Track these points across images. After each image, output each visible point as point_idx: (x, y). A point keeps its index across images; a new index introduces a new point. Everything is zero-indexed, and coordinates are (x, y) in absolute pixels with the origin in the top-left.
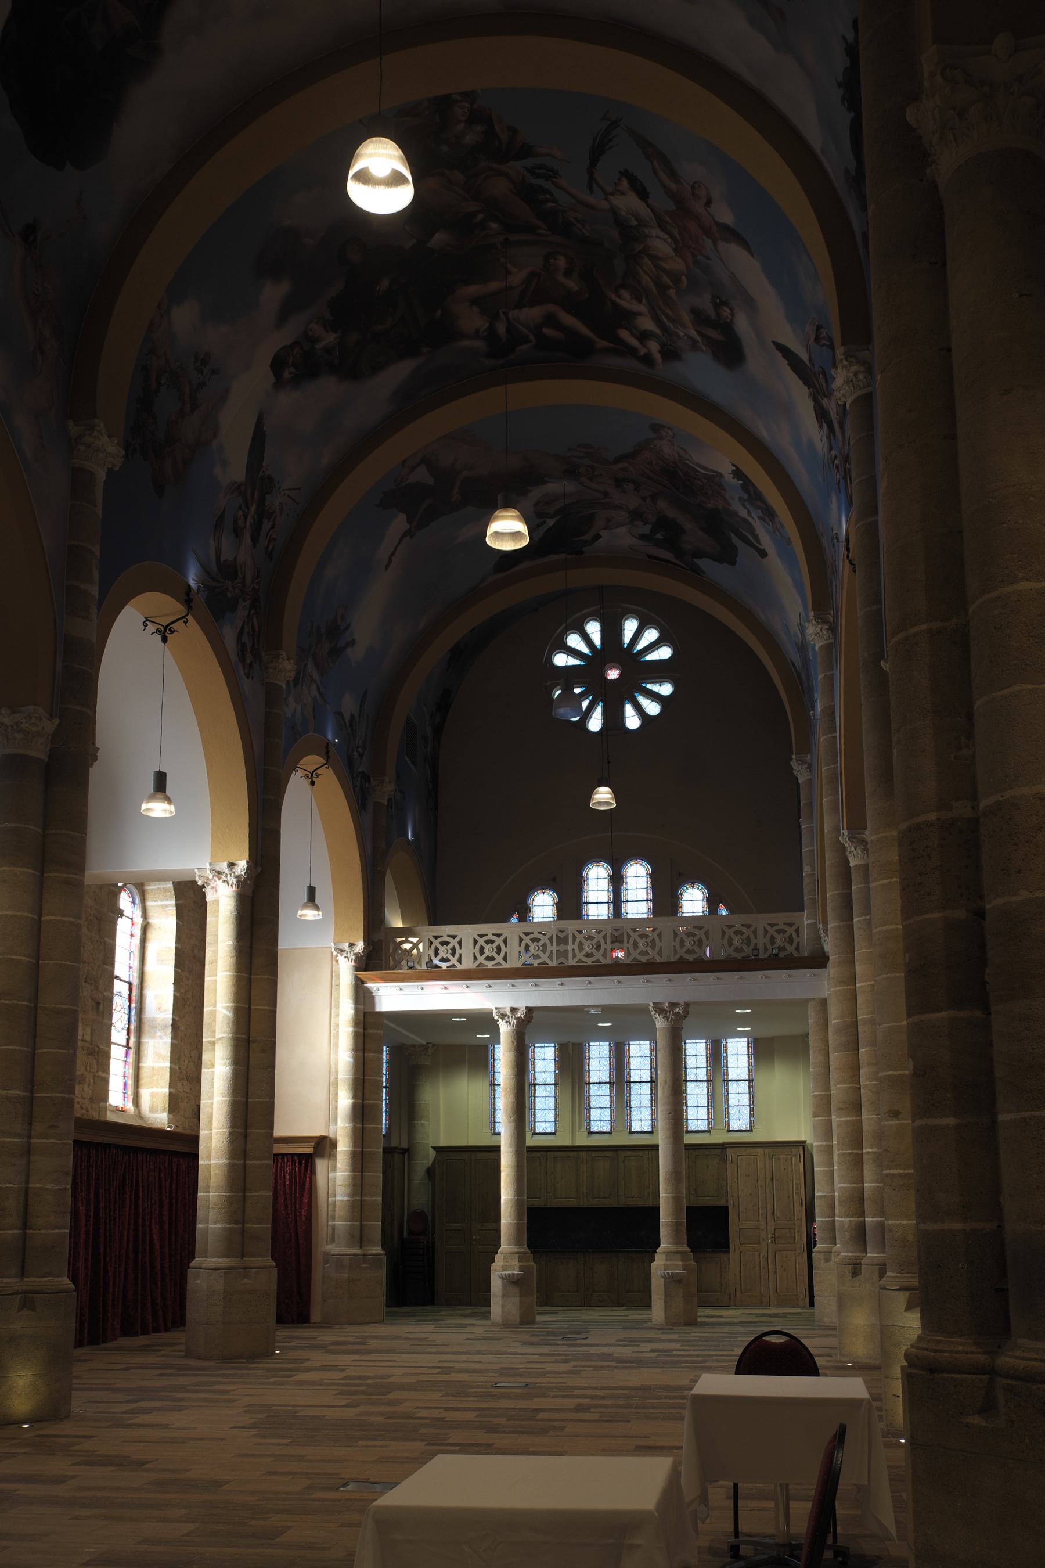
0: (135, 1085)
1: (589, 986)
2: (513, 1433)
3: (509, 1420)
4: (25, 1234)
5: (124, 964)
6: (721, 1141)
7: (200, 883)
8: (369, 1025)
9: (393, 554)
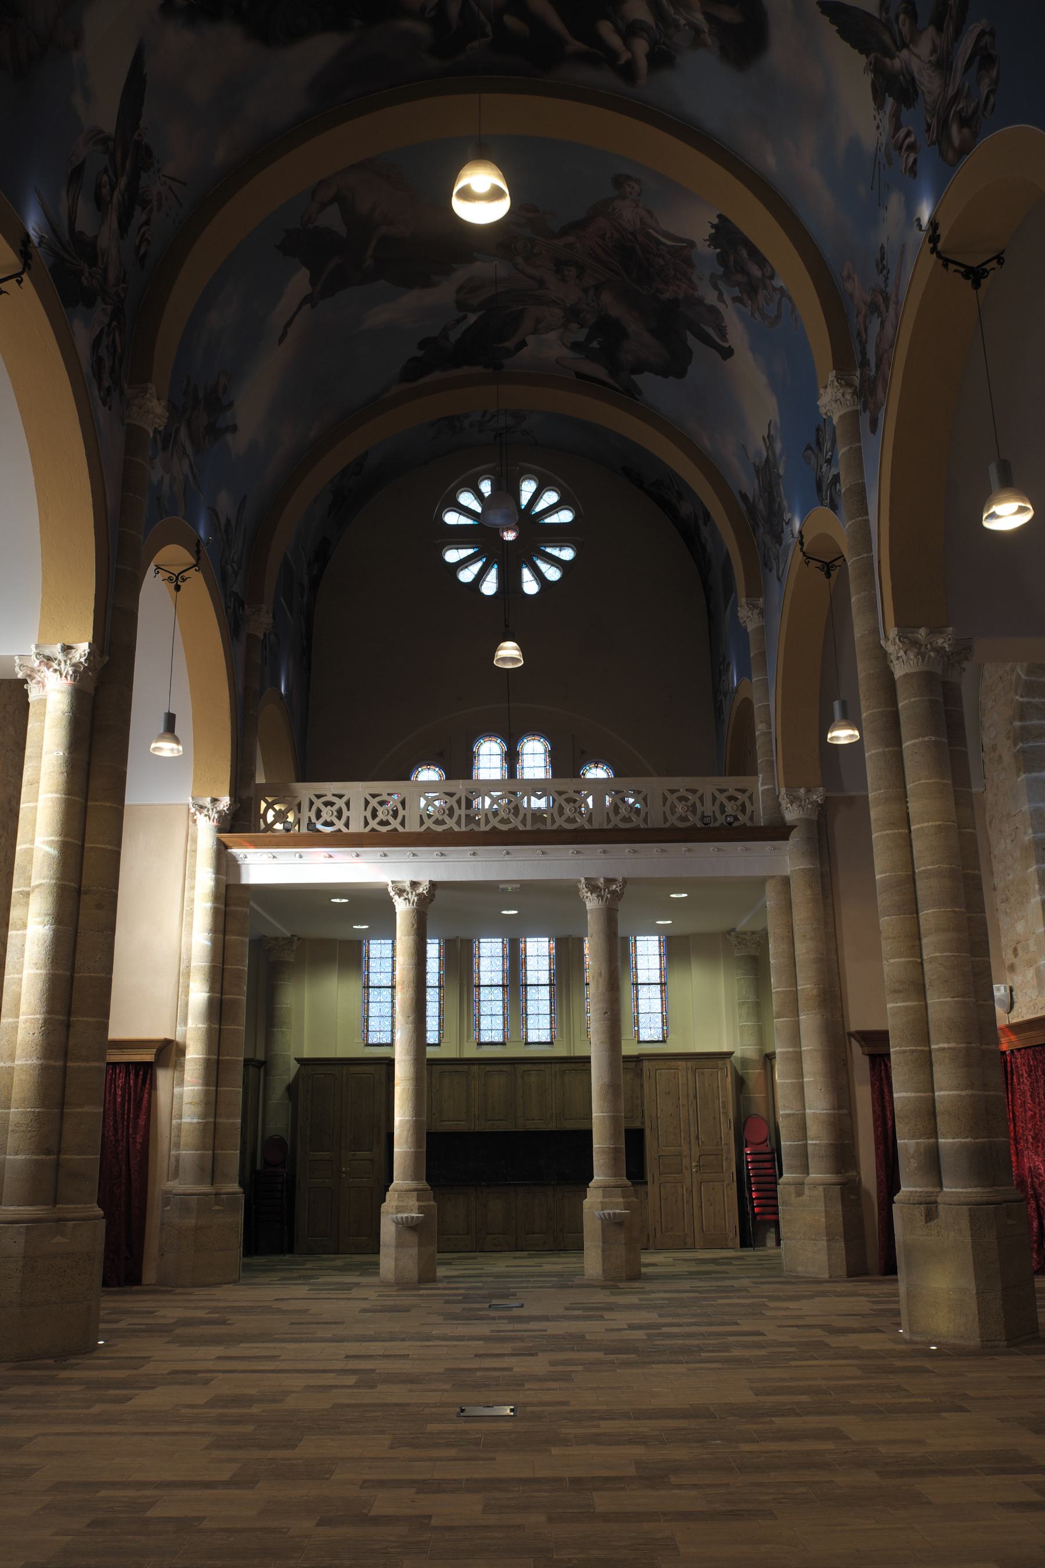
1: (507, 858)
6: (636, 1053)
8: (233, 899)
9: (289, 324)
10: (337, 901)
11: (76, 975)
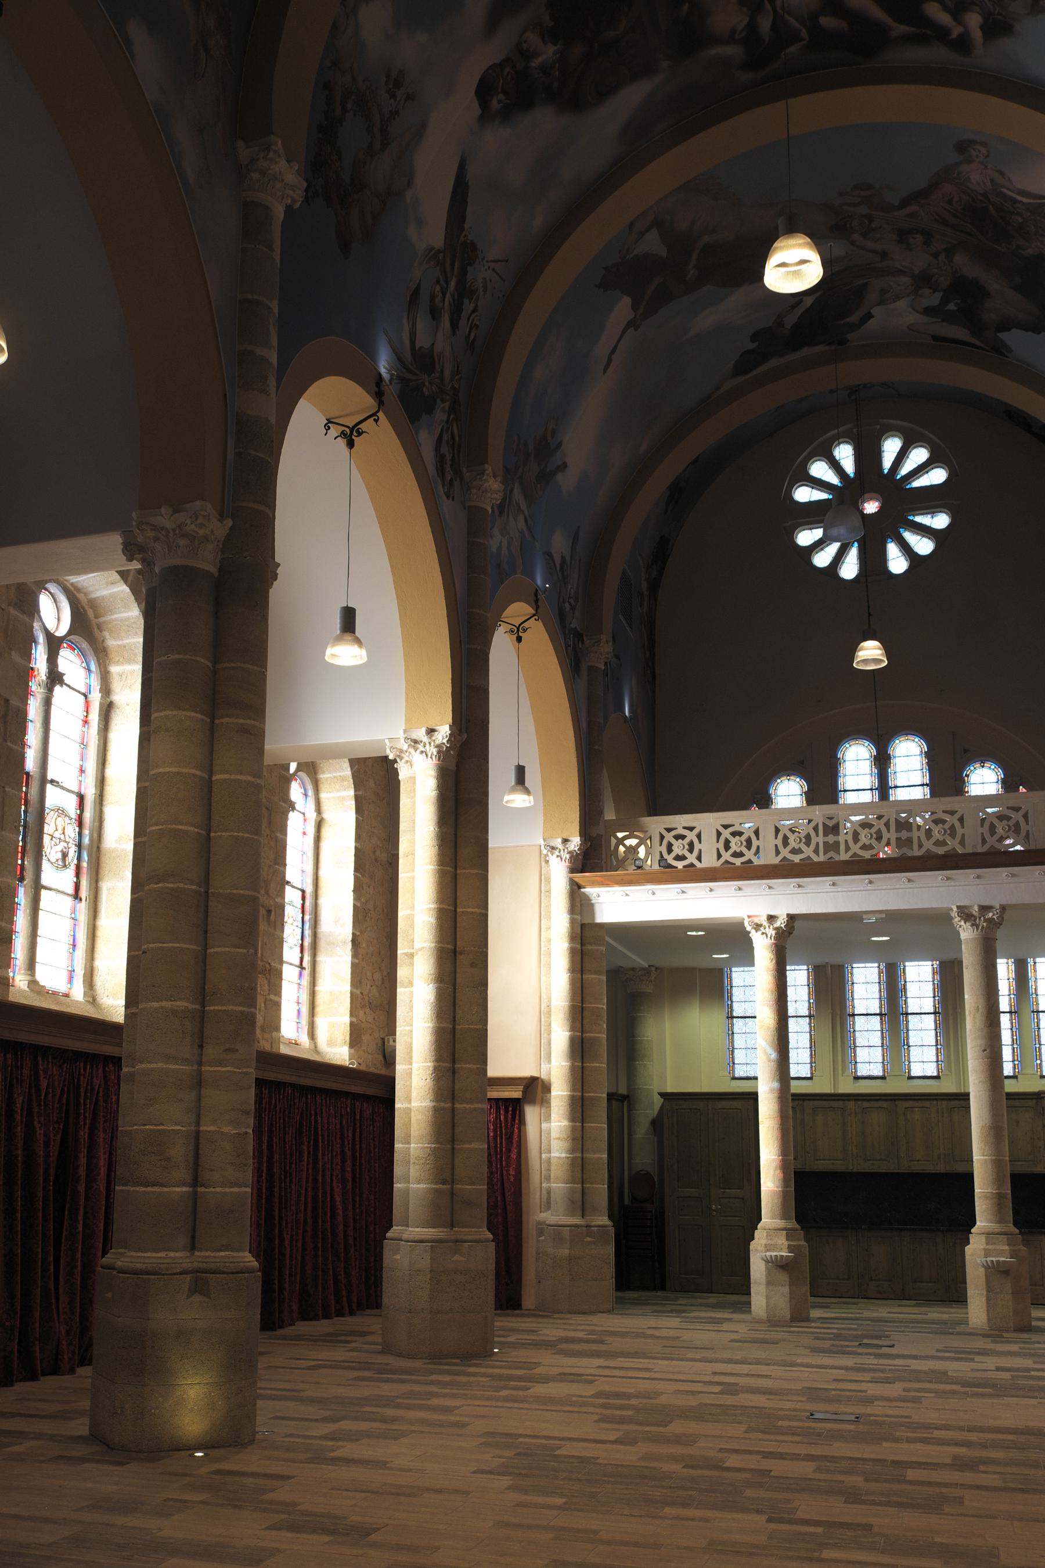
0: (313, 1015)
1: (870, 887)
2: (888, 1504)
3: (866, 1480)
4: (195, 1193)
5: (296, 867)
6: (1036, 1090)
7: (391, 757)
8: (588, 938)
9: (613, 351)
10: (694, 933)
11: (457, 1027)
